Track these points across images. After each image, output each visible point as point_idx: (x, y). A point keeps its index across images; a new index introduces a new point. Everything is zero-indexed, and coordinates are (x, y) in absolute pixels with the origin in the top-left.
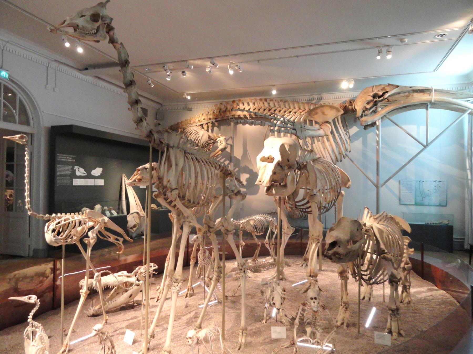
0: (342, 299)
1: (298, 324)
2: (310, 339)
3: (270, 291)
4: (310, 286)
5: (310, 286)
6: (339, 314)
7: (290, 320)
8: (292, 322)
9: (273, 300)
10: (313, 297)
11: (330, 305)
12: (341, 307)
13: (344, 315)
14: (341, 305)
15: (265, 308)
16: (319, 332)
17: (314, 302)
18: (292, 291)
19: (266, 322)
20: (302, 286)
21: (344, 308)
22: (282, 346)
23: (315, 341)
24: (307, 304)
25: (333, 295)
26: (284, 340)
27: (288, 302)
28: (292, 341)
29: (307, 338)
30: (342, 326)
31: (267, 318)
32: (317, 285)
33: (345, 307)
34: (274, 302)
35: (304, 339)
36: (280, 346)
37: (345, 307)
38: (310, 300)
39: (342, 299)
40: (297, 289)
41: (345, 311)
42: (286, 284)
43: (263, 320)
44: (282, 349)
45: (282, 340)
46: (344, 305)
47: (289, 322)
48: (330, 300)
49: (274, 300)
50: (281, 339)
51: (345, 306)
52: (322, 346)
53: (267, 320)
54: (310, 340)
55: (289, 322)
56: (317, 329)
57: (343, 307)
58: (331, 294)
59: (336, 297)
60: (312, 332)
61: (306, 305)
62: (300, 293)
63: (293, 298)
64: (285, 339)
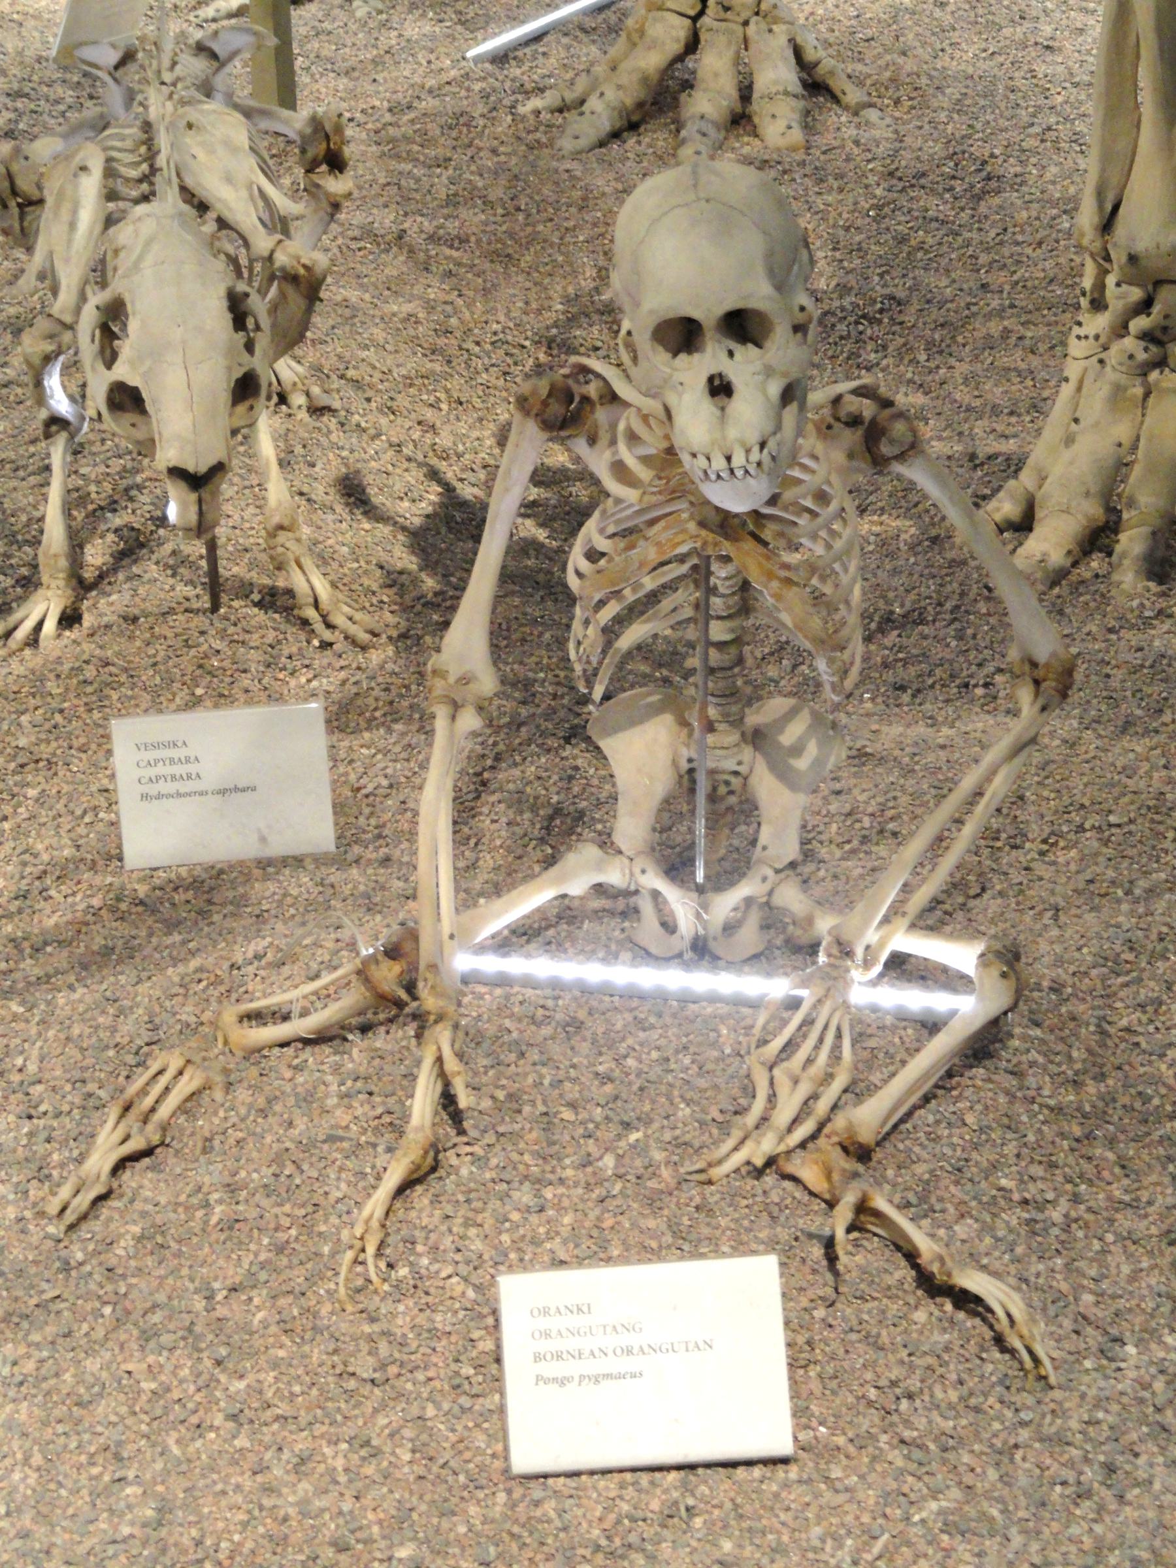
0: (1107, 225)
1: (487, 683)
2: (654, 880)
3: (90, 186)
4: (693, 45)
5: (693, 45)
6: (1060, 410)
7: (404, 559)
8: (430, 583)
9: (110, 358)
10: (707, 312)
11: (938, 283)
12: (1098, 323)
13: (1122, 431)
14: (1098, 304)
15: (56, 422)
16: (784, 774)
17: (720, 388)
18: (461, 120)
19: (70, 619)
20: (589, 51)
21: (1129, 343)
22: (256, 1017)
23: (726, 903)
24: (612, 397)
25: (979, 149)
26: (301, 884)
27: (393, 288)
28: (392, 952)
29: (614, 876)
30: (1096, 563)
31: (96, 555)
32: (779, 40)
33: (1140, 323)
34: (122, 371)
35: (577, 888)
36: (229, 1015)
37: (1140, 323)
38: (658, 359)
39: (1107, 225)
40: (527, 93)
41: (1144, 370)
42: (389, 39)
43: (29, 583)
44: (255, 1053)
45: (264, 891)
46: (1136, 294)
47: (394, 580)
48: (936, 206)
49: (126, 349)
50: (268, 866)
51: (1145, 306)
52: (835, 978)
53: (82, 586)
54: (656, 894)
55: (394, 580)
56: (757, 738)
57: (1120, 330)
58: (957, 126)
59: (1012, 168)
60: (688, 779)
61: (601, 415)
62: (567, 144)
63: (472, 218)
64: (320, 860)
